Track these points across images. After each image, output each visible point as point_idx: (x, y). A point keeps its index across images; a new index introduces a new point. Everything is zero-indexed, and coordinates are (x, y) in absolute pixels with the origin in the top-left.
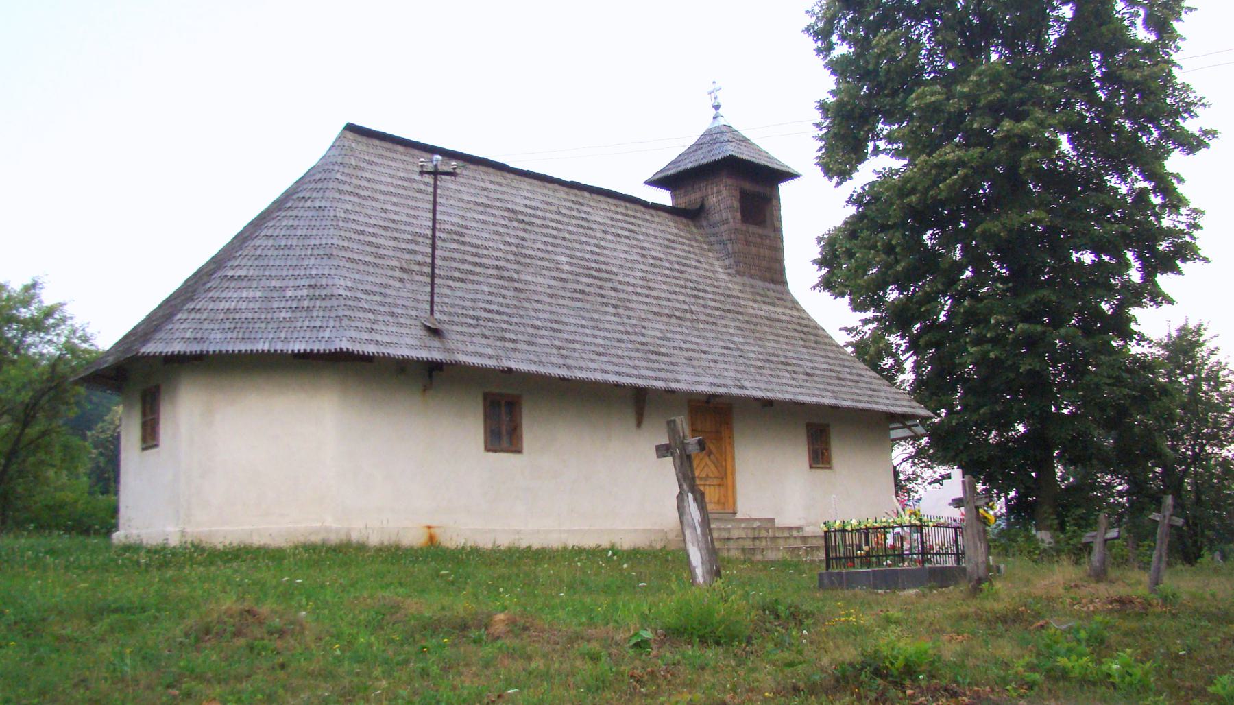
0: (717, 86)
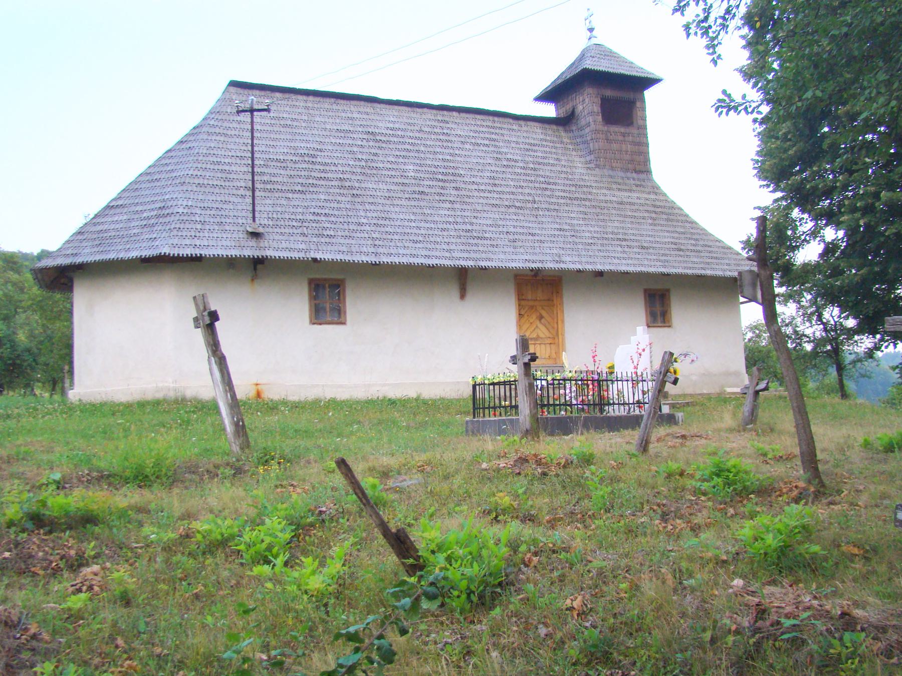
0: (590, 12)
